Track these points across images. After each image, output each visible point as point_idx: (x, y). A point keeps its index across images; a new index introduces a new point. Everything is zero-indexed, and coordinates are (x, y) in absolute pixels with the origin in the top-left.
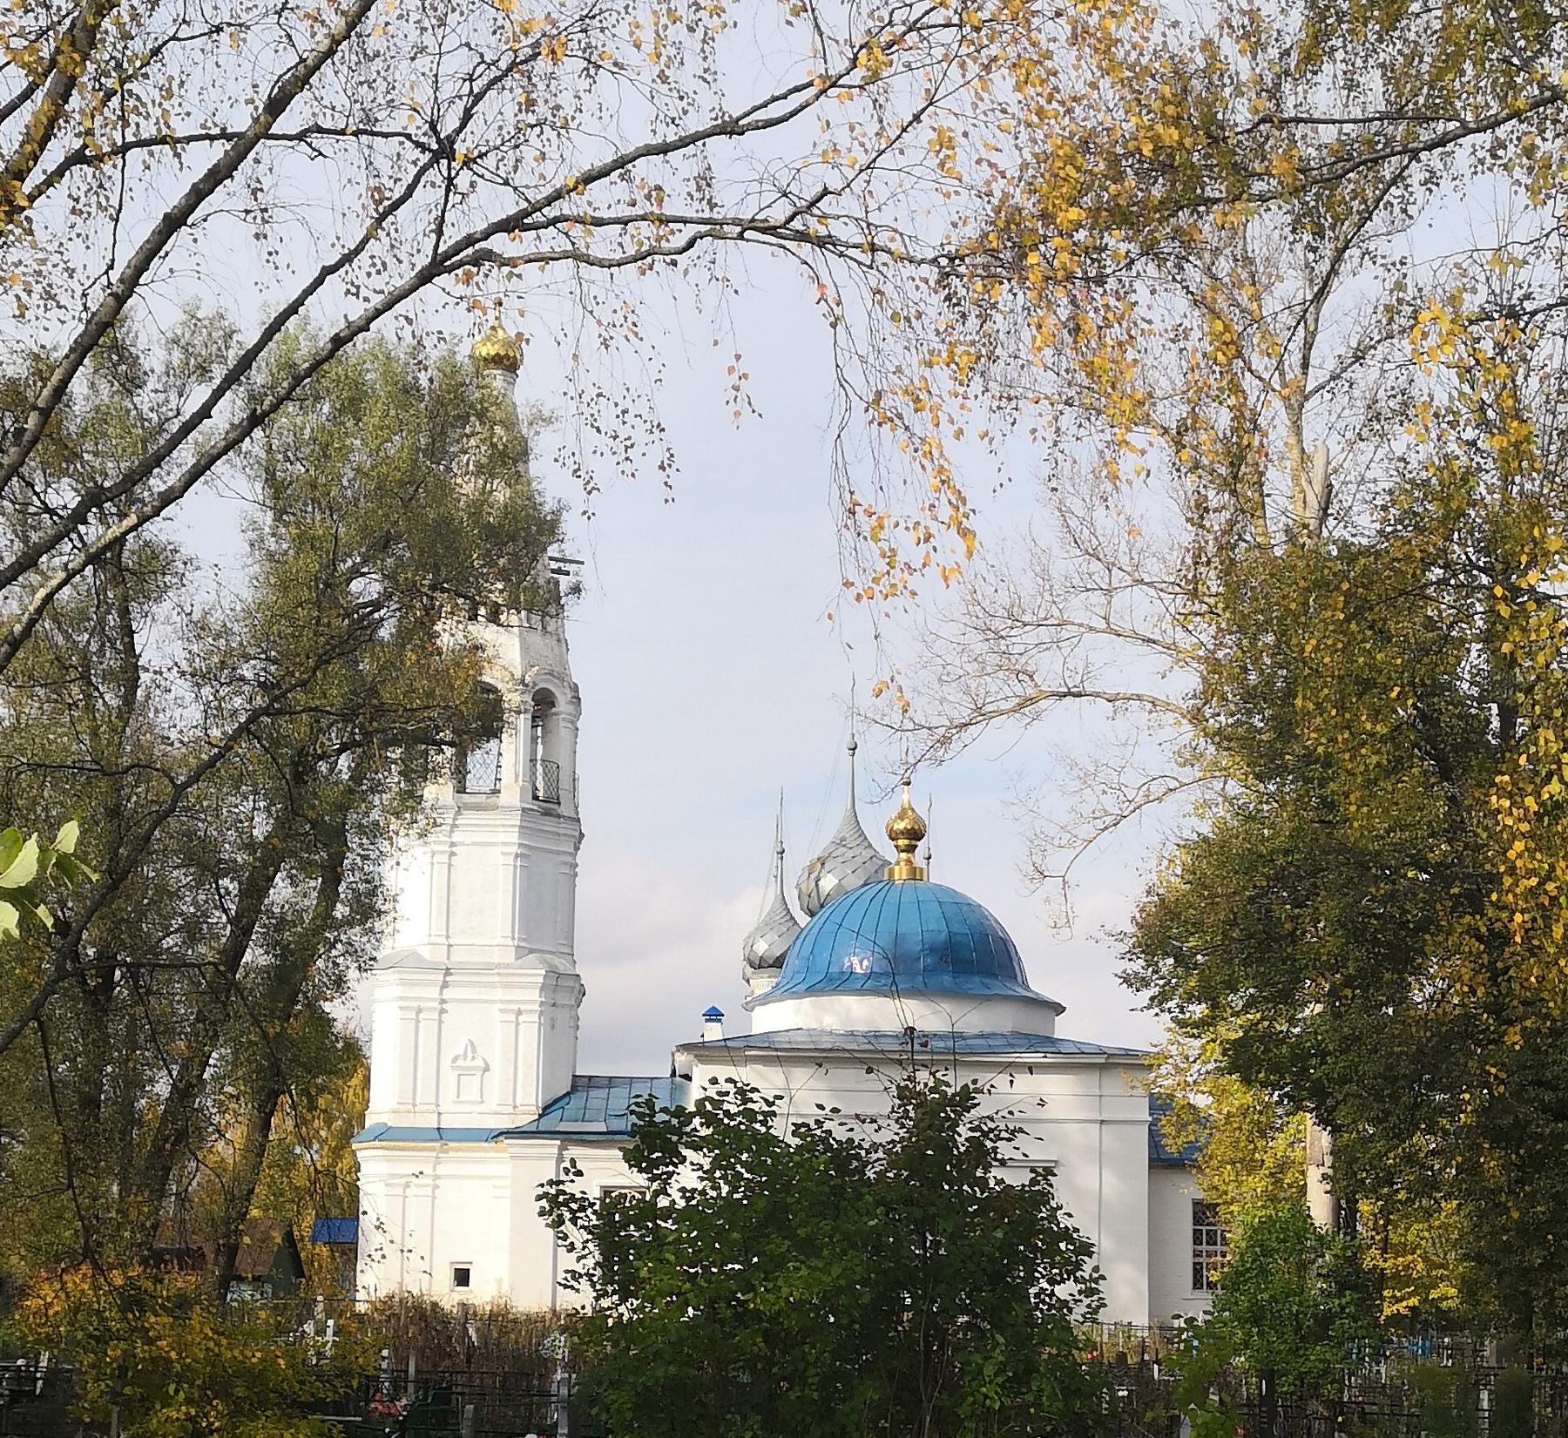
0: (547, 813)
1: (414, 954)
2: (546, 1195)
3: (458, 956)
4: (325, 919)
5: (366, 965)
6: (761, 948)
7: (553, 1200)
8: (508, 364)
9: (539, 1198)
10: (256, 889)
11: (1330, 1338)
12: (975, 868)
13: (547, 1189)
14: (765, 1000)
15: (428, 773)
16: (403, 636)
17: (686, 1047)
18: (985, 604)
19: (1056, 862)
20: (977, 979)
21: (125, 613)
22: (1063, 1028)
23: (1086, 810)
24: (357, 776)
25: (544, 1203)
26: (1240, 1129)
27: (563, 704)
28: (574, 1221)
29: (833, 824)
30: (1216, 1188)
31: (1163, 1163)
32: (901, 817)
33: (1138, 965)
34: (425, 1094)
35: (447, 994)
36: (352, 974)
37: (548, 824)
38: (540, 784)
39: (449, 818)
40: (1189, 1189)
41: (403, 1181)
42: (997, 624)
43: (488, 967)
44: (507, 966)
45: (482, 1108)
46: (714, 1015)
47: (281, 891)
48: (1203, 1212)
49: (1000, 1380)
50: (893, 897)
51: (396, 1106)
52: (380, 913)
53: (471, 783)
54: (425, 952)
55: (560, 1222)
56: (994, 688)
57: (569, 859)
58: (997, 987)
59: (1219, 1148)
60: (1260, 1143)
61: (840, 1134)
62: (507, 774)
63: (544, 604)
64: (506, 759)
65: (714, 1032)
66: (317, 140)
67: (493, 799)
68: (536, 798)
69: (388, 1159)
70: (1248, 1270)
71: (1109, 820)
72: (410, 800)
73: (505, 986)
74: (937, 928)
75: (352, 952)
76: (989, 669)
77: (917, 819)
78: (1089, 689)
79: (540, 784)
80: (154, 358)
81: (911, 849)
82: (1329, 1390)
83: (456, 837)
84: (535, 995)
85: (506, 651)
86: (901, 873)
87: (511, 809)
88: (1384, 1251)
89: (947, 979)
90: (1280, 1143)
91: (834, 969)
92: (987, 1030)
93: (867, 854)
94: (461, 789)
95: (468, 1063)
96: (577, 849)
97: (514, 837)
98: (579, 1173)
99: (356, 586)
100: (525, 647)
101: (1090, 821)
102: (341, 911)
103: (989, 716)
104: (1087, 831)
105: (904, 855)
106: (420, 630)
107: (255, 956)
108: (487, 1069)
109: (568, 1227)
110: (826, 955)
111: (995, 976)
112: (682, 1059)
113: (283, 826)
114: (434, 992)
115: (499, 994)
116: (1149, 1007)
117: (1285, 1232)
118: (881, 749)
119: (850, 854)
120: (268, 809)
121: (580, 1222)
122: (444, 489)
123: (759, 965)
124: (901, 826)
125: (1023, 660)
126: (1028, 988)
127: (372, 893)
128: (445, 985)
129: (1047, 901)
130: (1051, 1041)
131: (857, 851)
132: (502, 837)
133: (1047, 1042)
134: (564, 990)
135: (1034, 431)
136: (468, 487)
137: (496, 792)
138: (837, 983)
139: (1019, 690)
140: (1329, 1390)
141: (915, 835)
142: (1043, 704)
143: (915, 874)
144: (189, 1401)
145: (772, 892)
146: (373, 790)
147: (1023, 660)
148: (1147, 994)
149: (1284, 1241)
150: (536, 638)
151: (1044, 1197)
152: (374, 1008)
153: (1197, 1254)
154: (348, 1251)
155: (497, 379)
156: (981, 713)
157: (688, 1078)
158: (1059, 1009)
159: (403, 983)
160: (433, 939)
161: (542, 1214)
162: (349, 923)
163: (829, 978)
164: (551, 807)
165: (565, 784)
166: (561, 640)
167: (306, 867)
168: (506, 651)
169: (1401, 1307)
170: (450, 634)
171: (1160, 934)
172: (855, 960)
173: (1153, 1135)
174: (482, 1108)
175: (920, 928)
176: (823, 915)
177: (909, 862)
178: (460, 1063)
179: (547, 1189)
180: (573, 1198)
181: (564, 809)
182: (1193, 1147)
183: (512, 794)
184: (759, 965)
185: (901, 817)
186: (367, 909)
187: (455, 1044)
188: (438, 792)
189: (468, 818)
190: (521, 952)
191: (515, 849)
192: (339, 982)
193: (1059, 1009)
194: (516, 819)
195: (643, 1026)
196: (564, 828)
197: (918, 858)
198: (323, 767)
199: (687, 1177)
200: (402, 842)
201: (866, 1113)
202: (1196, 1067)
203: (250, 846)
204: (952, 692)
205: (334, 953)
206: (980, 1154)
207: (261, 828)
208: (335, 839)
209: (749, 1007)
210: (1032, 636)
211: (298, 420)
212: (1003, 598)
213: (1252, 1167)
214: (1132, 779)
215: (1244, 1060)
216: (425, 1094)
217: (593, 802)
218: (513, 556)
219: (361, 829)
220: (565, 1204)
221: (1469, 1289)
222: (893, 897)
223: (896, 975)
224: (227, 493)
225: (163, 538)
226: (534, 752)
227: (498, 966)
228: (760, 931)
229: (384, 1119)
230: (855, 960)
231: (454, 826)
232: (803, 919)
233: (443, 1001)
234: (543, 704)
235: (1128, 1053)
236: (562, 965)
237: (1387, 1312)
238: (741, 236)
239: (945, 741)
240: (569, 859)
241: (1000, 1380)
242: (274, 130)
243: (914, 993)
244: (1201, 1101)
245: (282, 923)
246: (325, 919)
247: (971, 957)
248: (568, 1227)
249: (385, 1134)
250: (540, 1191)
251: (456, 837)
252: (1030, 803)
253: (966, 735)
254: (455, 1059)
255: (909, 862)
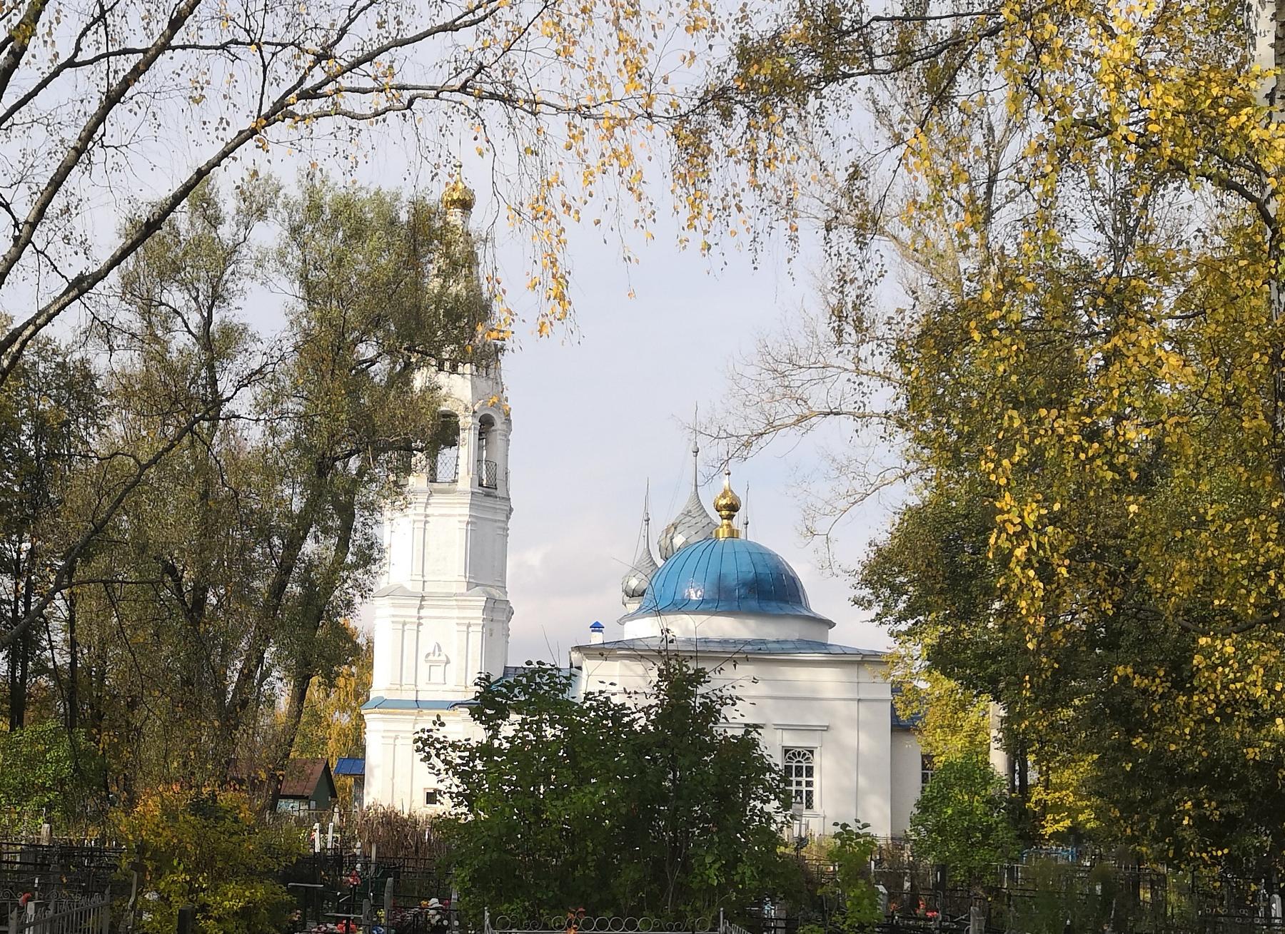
0: (488, 495)
1: (401, 587)
2: (420, 738)
3: (430, 588)
4: (339, 563)
5: (365, 592)
6: (634, 583)
7: (425, 742)
8: (466, 205)
9: (416, 741)
10: (294, 544)
11: (989, 845)
12: (772, 531)
13: (421, 734)
14: (631, 617)
15: (408, 470)
16: (391, 382)
17: (578, 649)
18: (774, 354)
19: (821, 525)
20: (774, 604)
21: (211, 368)
22: (833, 637)
23: (843, 490)
24: (361, 473)
25: (419, 744)
26: (947, 705)
27: (499, 424)
28: (438, 755)
29: (683, 502)
30: (929, 744)
31: (900, 728)
32: (724, 496)
33: (866, 592)
34: (408, 678)
35: (423, 613)
36: (358, 599)
37: (489, 502)
38: (484, 477)
39: (422, 498)
40: (914, 748)
41: (393, 735)
42: (781, 368)
43: (448, 596)
44: (462, 595)
45: (445, 687)
46: (597, 627)
47: (309, 547)
48: (927, 759)
49: (717, 866)
50: (717, 550)
51: (389, 686)
52: (375, 560)
53: (440, 477)
54: (409, 586)
55: (428, 757)
56: (780, 409)
57: (502, 525)
58: (788, 609)
59: (933, 716)
60: (961, 715)
61: (616, 700)
62: (462, 470)
63: (486, 359)
64: (461, 458)
65: (597, 639)
66: (233, 49)
67: (453, 486)
68: (481, 485)
69: (384, 720)
70: (936, 798)
71: (857, 497)
72: (398, 488)
73: (459, 607)
74: (747, 570)
75: (357, 585)
76: (778, 398)
77: (735, 498)
78: (844, 410)
79: (484, 477)
80: (229, 205)
81: (730, 517)
82: (989, 879)
83: (429, 511)
84: (479, 614)
85: (458, 390)
86: (723, 533)
87: (465, 493)
88: (1046, 788)
89: (754, 604)
90: (974, 716)
91: (678, 597)
92: (782, 638)
93: (705, 521)
94: (433, 479)
95: (436, 658)
96: (508, 518)
97: (466, 511)
98: (442, 724)
99: (361, 348)
100: (474, 387)
101: (838, 499)
102: (350, 558)
103: (777, 429)
104: (842, 504)
105: (725, 521)
106: (401, 379)
107: (294, 589)
108: (448, 662)
109: (434, 760)
110: (673, 588)
111: (787, 602)
112: (575, 655)
113: (313, 505)
114: (414, 612)
115: (456, 613)
116: (873, 621)
117: (971, 772)
118: (714, 451)
119: (694, 521)
120: (301, 493)
121: (442, 757)
122: (418, 286)
123: (633, 594)
124: (723, 502)
125: (800, 391)
126: (810, 610)
127: (371, 547)
128: (421, 607)
129: (816, 551)
130: (825, 645)
131: (698, 519)
132: (458, 511)
133: (822, 646)
134: (498, 611)
135: (637, 221)
136: (434, 285)
137: (455, 481)
138: (681, 606)
139: (798, 411)
140: (989, 879)
141: (733, 508)
142: (814, 420)
143: (733, 534)
144: (186, 870)
145: (643, 545)
146: (371, 481)
147: (800, 391)
148: (871, 614)
149: (960, 779)
150: (484, 384)
151: (754, 744)
152: (375, 619)
153: (809, 784)
154: (360, 781)
155: (455, 217)
156: (772, 426)
157: (580, 668)
158: (831, 624)
159: (394, 606)
160: (414, 578)
161: (418, 750)
162: (355, 566)
163: (674, 603)
164: (490, 489)
165: (500, 475)
166: (497, 382)
167: (326, 531)
168: (458, 390)
169: (1060, 827)
170: (419, 380)
171: (880, 574)
172: (692, 592)
173: (893, 709)
174: (445, 687)
175: (737, 569)
176: (671, 561)
177: (729, 525)
178: (431, 658)
179: (421, 734)
180: (437, 740)
181: (499, 492)
182: (915, 717)
183: (465, 483)
184: (633, 594)
185: (724, 496)
186: (368, 557)
187: (427, 646)
188: (417, 481)
189: (436, 499)
190: (470, 586)
191: (467, 519)
192: (349, 604)
193: (831, 624)
194: (468, 499)
195: (539, 636)
196: (499, 504)
197: (737, 522)
198: (339, 464)
199: (507, 730)
200: (387, 513)
201: (627, 685)
202: (918, 663)
203: (289, 516)
204: (752, 413)
205: (346, 586)
206: (710, 712)
207: (297, 505)
208: (347, 513)
209: (622, 622)
210: (806, 375)
211: (322, 243)
212: (786, 350)
213: (955, 730)
214: (873, 470)
215: (941, 659)
216: (408, 678)
217: (518, 489)
218: (462, 328)
219: (365, 507)
220: (432, 744)
221: (1100, 813)
222: (717, 550)
223: (724, 599)
224: (275, 290)
225: (235, 321)
226: (480, 455)
227: (455, 595)
228: (636, 569)
229: (381, 694)
230: (692, 592)
231: (427, 504)
232: (660, 562)
233: (420, 618)
234: (486, 424)
235: (876, 654)
236: (497, 594)
237: (1050, 830)
238: (437, 97)
239: (748, 445)
240: (502, 525)
241: (717, 866)
242: (173, 43)
243: (729, 613)
244: (923, 685)
245: (310, 566)
246: (339, 563)
247: (771, 590)
248: (434, 760)
249: (382, 704)
250: (417, 736)
251: (429, 511)
252: (804, 485)
253: (762, 441)
254: (428, 655)
255: (729, 525)
